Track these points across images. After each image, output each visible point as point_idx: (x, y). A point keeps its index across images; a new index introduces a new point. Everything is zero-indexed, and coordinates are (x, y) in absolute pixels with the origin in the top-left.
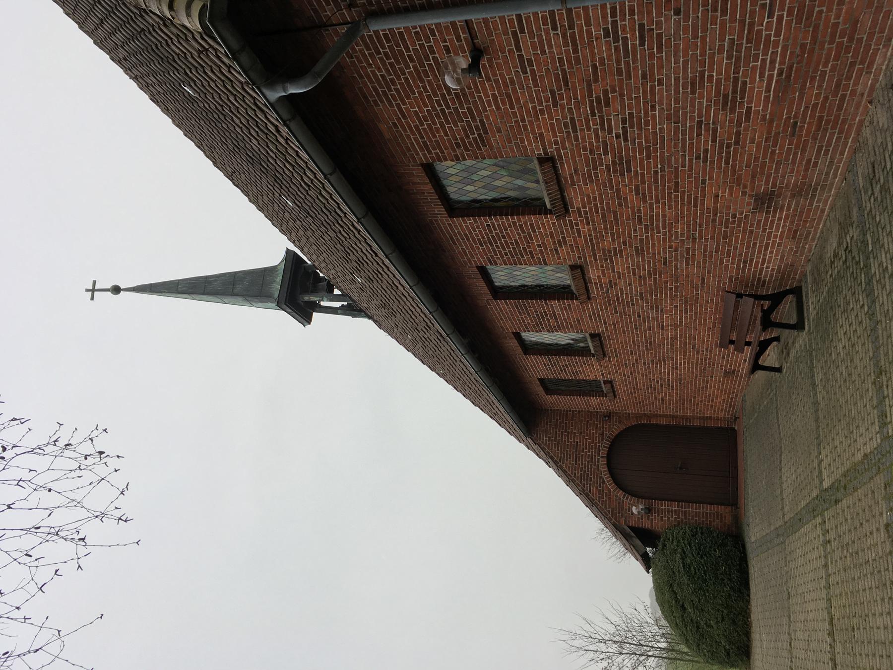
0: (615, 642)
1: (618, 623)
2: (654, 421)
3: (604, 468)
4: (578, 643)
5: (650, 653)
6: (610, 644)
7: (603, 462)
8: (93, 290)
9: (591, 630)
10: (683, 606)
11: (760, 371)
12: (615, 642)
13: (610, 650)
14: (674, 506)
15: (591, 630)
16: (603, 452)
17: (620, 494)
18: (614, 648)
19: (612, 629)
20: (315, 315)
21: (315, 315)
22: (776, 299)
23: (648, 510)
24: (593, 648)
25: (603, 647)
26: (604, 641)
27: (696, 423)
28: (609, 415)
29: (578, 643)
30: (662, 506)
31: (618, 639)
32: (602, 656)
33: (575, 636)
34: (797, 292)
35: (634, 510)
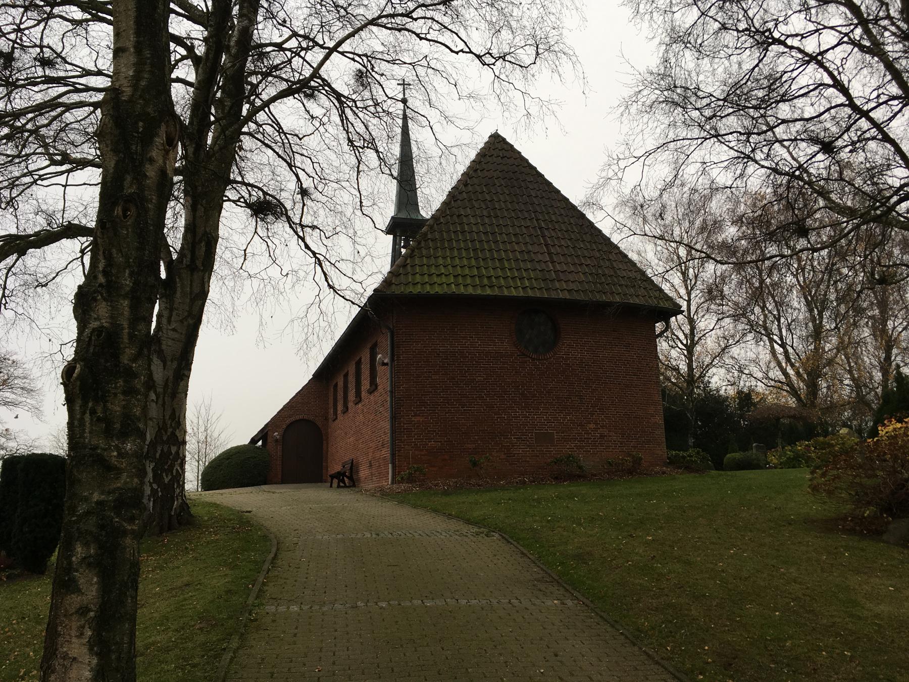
0: (206, 438)
1: (220, 439)
2: (324, 442)
3: (298, 418)
4: (203, 411)
5: (200, 462)
6: (205, 434)
7: (301, 417)
8: (404, 84)
9: (213, 421)
10: (228, 459)
11: (76, 324)
12: (206, 438)
13: (200, 434)
14: (280, 453)
15: (213, 421)
16: (306, 417)
17: (284, 427)
18: (202, 438)
19: (215, 435)
20: (392, 236)
21: (392, 236)
22: (351, 478)
23: (277, 441)
24: (201, 422)
25: (202, 429)
26: (206, 430)
27: (324, 464)
28: (327, 419)
29: (203, 411)
30: (279, 448)
31: (209, 440)
32: (195, 429)
33: (208, 411)
34: (354, 486)
35: (276, 434)
